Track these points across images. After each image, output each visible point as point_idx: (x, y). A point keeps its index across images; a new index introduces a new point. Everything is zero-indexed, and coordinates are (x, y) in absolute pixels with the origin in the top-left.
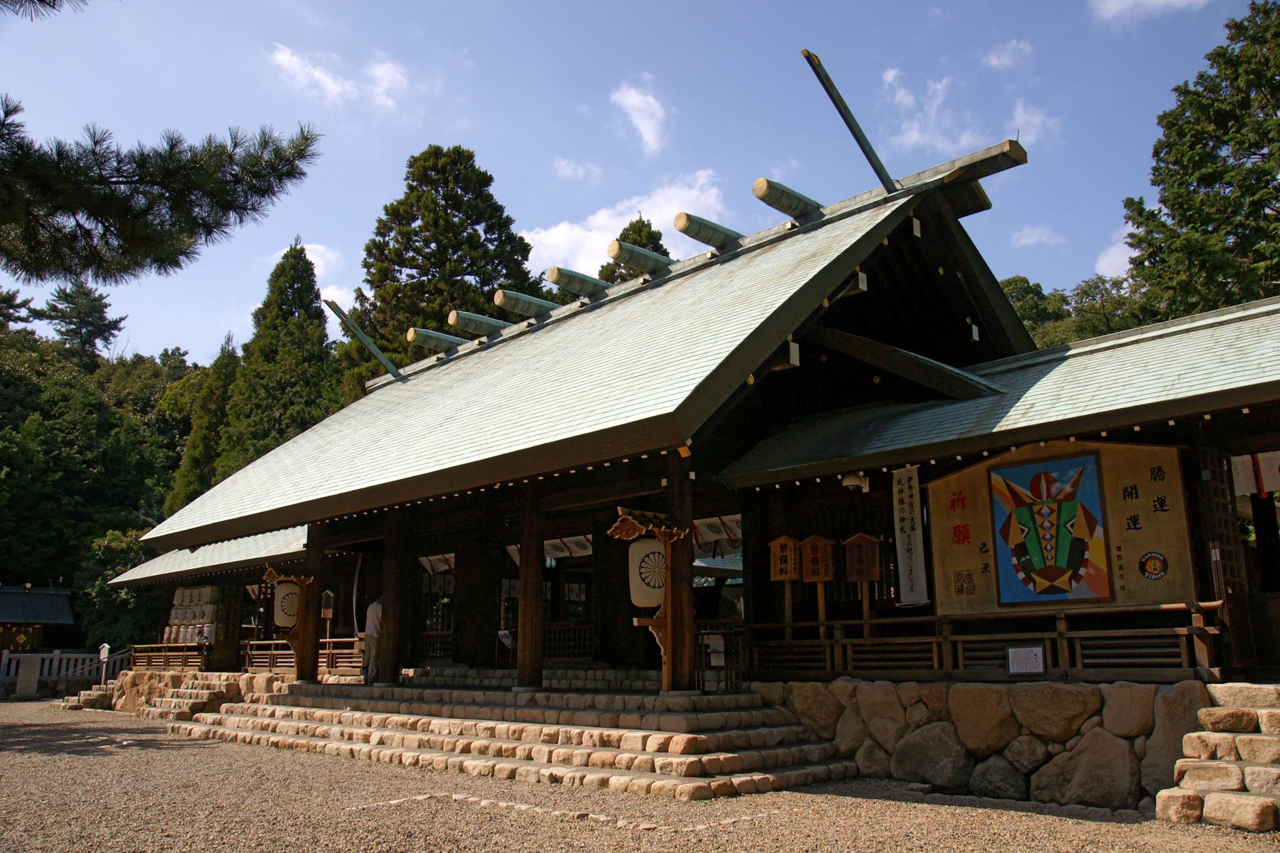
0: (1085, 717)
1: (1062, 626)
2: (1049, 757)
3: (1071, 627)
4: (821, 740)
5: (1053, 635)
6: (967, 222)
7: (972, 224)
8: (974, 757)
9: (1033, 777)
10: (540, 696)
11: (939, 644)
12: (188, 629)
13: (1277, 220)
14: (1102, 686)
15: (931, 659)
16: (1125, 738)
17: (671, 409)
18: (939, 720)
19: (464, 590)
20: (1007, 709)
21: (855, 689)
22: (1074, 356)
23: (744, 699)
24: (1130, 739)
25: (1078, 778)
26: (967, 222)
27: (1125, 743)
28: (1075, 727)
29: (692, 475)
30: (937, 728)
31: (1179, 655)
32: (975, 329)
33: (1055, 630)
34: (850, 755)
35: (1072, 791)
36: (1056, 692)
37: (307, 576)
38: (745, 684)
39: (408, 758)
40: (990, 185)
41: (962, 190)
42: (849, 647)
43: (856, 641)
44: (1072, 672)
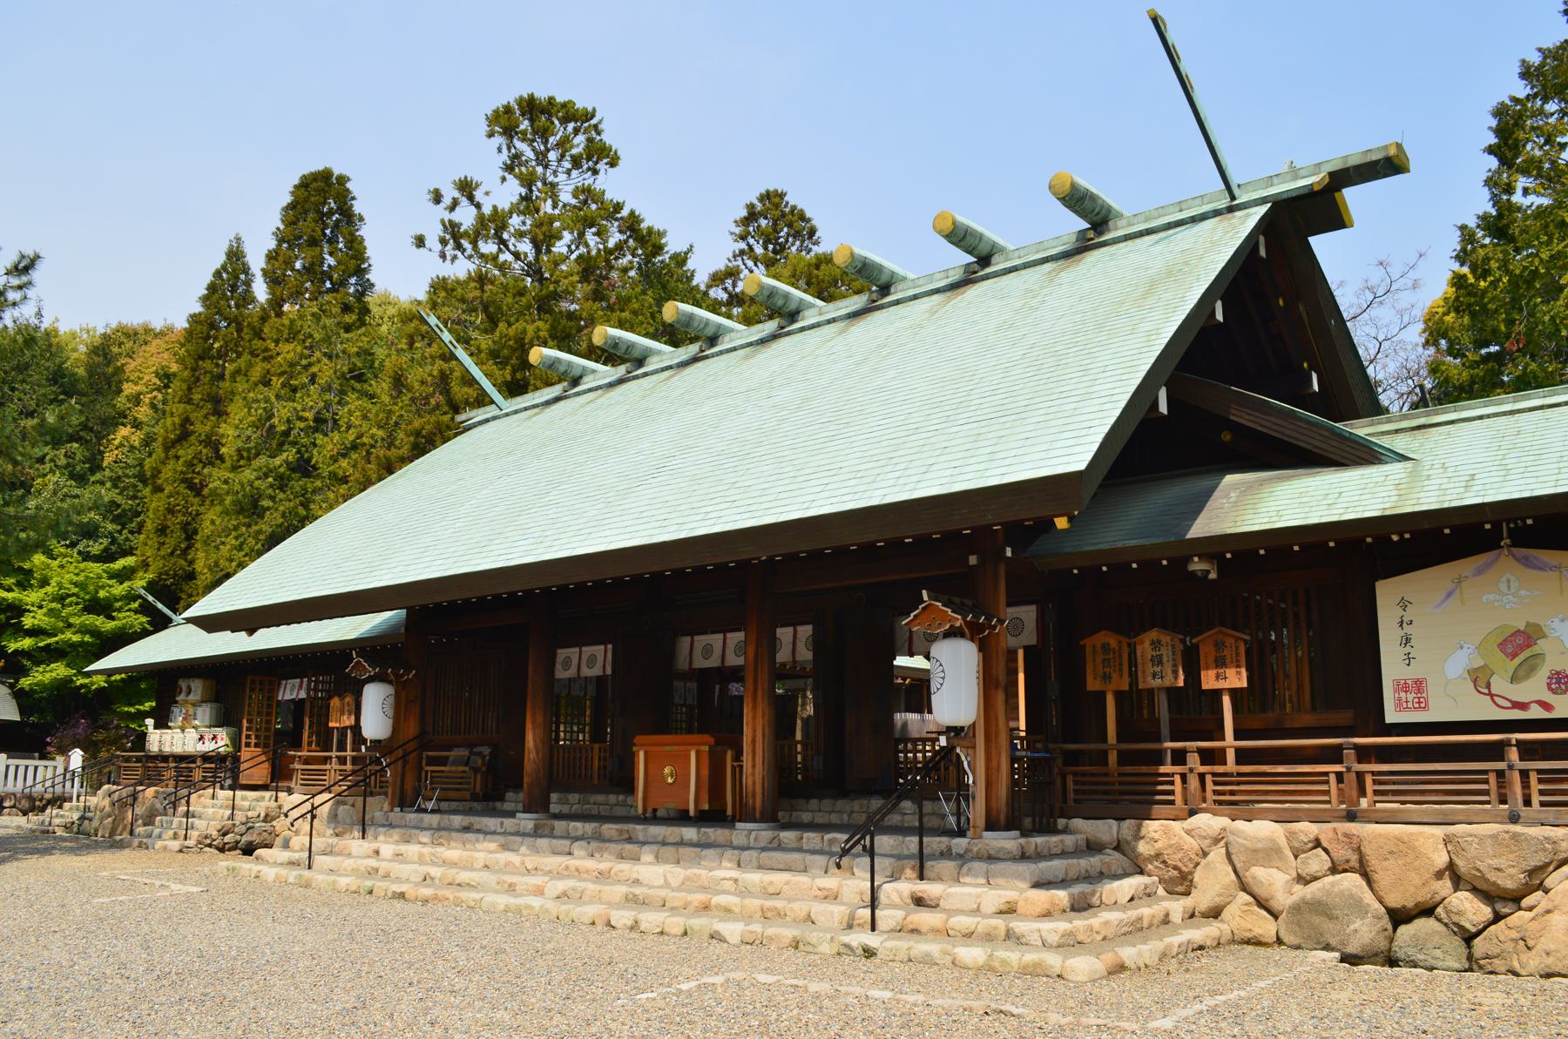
1: (1513, 754)
5: (1501, 765)
6: (1319, 243)
7: (1322, 245)
8: (1399, 917)
10: (788, 836)
11: (1184, 777)
17: (1082, 466)
19: (538, 698)
23: (1069, 840)
26: (1319, 243)
29: (1009, 553)
36: (1515, 836)
37: (408, 671)
38: (1061, 822)
39: (622, 918)
40: (1353, 197)
41: (1311, 210)
43: (1220, 769)
44: (1524, 812)
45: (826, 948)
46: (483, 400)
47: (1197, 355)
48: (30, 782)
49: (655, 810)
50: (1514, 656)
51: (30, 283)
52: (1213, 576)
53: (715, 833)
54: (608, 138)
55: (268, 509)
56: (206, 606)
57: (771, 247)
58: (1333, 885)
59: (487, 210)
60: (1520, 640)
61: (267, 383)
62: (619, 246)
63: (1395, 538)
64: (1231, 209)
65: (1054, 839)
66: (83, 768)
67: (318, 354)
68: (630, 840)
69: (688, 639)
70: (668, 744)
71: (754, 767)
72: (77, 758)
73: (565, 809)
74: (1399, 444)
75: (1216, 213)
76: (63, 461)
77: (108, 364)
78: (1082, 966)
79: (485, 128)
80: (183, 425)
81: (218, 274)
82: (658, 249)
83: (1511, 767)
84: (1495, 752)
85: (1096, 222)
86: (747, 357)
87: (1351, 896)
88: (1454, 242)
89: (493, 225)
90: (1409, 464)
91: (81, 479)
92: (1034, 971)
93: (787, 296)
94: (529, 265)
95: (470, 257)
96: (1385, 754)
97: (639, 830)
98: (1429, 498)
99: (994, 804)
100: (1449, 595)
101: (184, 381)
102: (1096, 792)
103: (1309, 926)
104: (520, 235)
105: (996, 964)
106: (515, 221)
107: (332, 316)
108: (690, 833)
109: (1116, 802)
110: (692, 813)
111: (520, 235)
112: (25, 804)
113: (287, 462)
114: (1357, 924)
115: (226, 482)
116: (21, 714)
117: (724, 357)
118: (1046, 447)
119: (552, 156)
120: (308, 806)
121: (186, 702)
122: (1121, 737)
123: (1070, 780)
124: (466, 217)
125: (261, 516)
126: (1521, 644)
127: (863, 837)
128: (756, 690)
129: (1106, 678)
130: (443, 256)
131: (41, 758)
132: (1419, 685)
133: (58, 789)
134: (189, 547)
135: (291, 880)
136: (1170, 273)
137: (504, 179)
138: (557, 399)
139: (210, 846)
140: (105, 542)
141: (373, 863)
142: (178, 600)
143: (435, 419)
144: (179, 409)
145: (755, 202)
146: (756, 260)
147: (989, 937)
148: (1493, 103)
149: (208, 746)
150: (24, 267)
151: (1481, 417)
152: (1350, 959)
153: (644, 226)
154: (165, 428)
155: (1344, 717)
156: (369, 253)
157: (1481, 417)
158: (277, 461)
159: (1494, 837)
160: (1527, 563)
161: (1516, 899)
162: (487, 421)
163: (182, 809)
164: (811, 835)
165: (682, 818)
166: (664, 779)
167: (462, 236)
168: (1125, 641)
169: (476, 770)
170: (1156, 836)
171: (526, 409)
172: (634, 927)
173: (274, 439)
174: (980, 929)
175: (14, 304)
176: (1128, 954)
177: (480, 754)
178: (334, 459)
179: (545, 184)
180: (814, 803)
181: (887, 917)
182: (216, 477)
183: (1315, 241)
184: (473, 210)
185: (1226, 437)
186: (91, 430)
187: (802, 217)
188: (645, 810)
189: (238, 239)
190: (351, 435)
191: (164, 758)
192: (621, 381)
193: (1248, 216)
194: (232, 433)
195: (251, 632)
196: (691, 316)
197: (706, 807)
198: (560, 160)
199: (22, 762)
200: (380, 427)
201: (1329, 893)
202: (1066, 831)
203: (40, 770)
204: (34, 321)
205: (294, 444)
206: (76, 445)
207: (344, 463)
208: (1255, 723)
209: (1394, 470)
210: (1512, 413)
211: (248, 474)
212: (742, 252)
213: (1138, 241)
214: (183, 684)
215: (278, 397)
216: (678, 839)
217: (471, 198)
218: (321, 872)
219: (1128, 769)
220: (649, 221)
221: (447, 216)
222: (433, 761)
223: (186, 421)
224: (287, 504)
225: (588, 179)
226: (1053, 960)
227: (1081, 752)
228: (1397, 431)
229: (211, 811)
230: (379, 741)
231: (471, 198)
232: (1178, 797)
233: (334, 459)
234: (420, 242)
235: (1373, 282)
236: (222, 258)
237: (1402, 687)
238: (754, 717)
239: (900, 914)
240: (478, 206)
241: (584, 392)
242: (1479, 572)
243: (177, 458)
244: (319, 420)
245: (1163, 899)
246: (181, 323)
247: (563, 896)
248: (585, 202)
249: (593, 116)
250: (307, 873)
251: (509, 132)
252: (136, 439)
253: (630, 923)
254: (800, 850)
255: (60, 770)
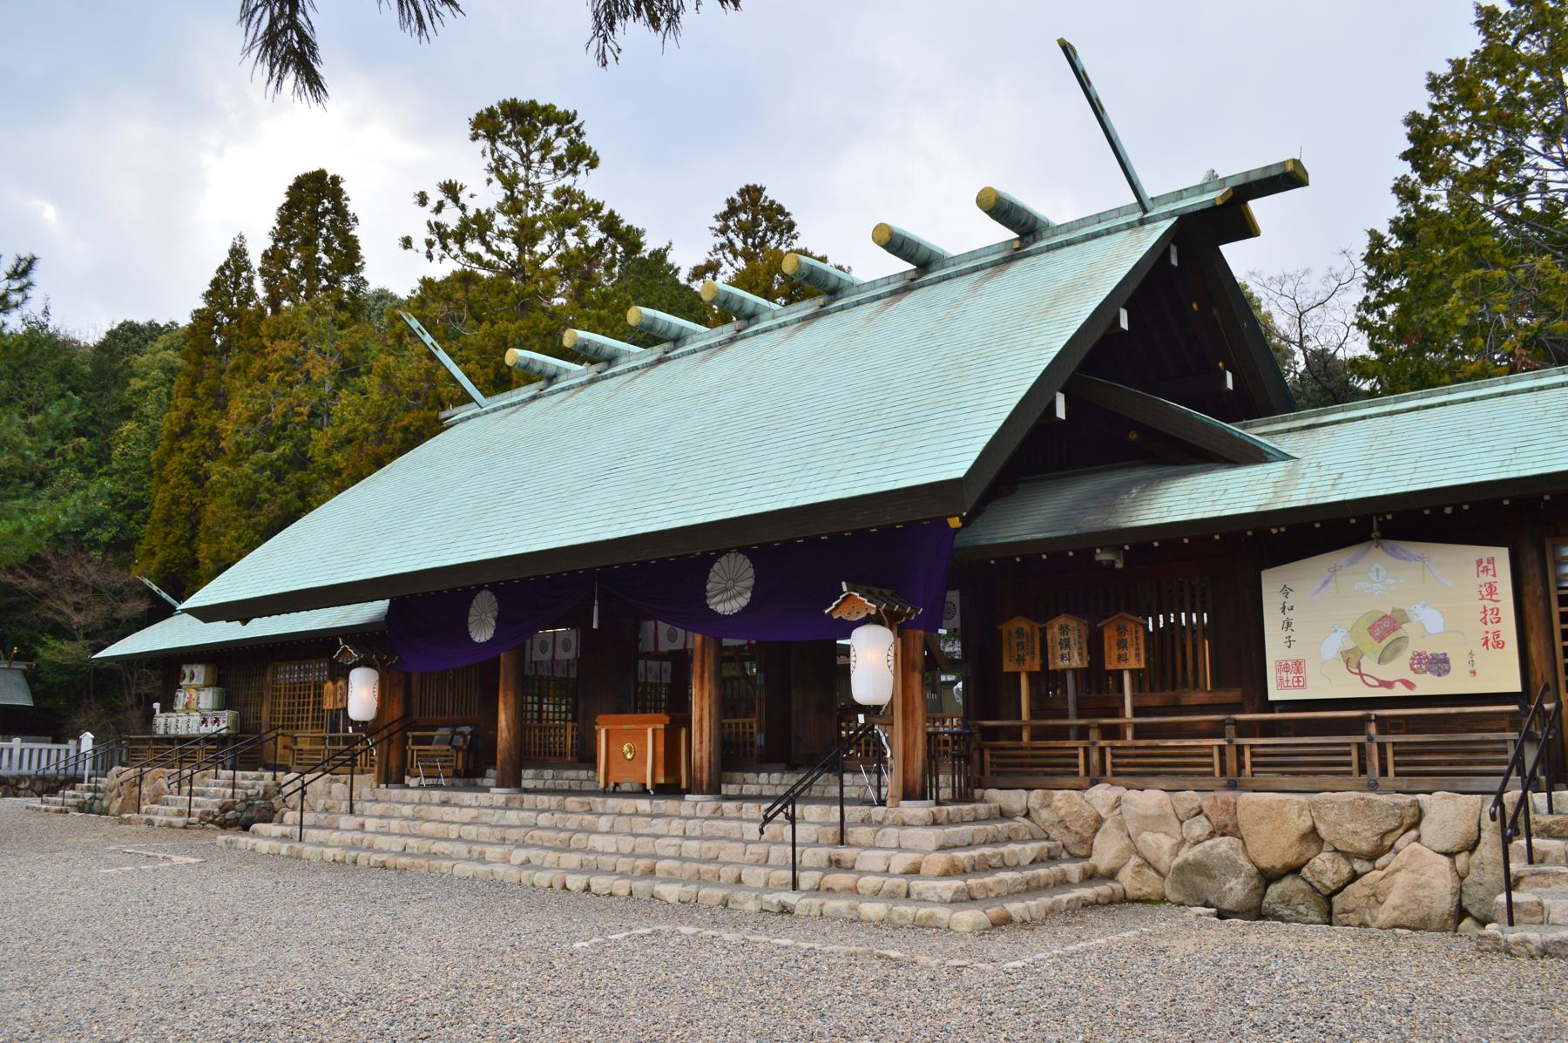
0: (1400, 831)
1: (1372, 729)
2: (1355, 876)
3: (1381, 732)
4: (1074, 857)
5: (1362, 739)
6: (1228, 250)
7: (1232, 252)
8: (1268, 877)
9: (1336, 898)
10: (729, 806)
11: (1086, 750)
12: (194, 711)
13: (5, 296)
14: (1420, 797)
15: (1212, 765)
16: (1445, 854)
17: (961, 474)
18: (1223, 835)
19: (537, 668)
20: (1309, 823)
21: (1119, 799)
22: (462, 420)
23: (981, 808)
24: (1450, 854)
25: (1393, 899)
26: (1228, 250)
27: (1445, 860)
28: (1387, 843)
30: (1223, 844)
31: (1349, 764)
32: (1229, 376)
33: (1362, 733)
34: (1111, 875)
35: (1384, 915)
36: (1369, 803)
38: (978, 792)
39: (575, 882)
41: (1228, 215)
42: (1108, 751)
43: (1118, 743)
44: (1382, 781)
45: (751, 906)
46: (468, 399)
47: (1094, 359)
48: (44, 765)
49: (616, 784)
50: (1381, 639)
51: (30, 284)
52: (1119, 565)
53: (666, 805)
54: (588, 140)
55: (265, 501)
56: (206, 596)
57: (750, 241)
58: (1212, 847)
59: (471, 213)
60: (1387, 625)
61: (263, 379)
62: (600, 244)
63: (1274, 531)
64: (1142, 222)
65: (966, 807)
66: (95, 751)
67: (311, 351)
68: (590, 811)
69: (652, 623)
70: (628, 723)
71: (701, 743)
72: (87, 739)
73: (540, 784)
74: (1286, 444)
75: (1130, 226)
76: (71, 455)
77: (114, 361)
78: (968, 917)
79: (469, 132)
80: (187, 419)
81: (221, 270)
82: (638, 246)
83: (1371, 739)
84: (1356, 727)
85: (1025, 230)
86: (703, 360)
87: (1228, 858)
88: (1362, 245)
89: (477, 226)
90: (1290, 463)
91: (87, 471)
92: (920, 925)
93: (742, 300)
94: (513, 264)
95: (455, 257)
96: (1269, 729)
97: (597, 802)
98: (1301, 494)
99: (910, 776)
100: (1326, 582)
101: (188, 375)
102: (1022, 765)
103: (1192, 885)
104: (502, 235)
105: (895, 917)
106: (501, 222)
107: (325, 313)
108: (643, 805)
109: (1029, 774)
110: (649, 786)
111: (502, 235)
112: (39, 786)
113: (282, 455)
114: (1233, 883)
115: (225, 475)
116: (35, 696)
117: (684, 360)
118: (936, 455)
119: (535, 156)
120: (298, 783)
121: (190, 686)
122: (1034, 714)
123: (987, 753)
124: (451, 218)
125: (260, 508)
126: (1387, 628)
127: (785, 806)
128: (703, 673)
129: (1021, 660)
130: (430, 257)
131: (54, 742)
132: (1299, 666)
133: (71, 771)
134: (193, 537)
135: (284, 852)
136: (1076, 286)
137: (490, 181)
138: (534, 398)
139: (212, 822)
140: (114, 530)
141: (358, 835)
142: (183, 588)
143: (414, 419)
144: (186, 403)
145: (736, 197)
146: (735, 254)
147: (892, 896)
148: (1405, 113)
149: (211, 729)
150: (22, 270)
151: (1364, 418)
152: (1222, 915)
153: (624, 225)
154: (169, 422)
155: (1232, 695)
156: (362, 252)
157: (1364, 418)
158: (274, 455)
159: (1351, 803)
160: (1393, 553)
161: (1372, 857)
162: (469, 418)
163: (186, 788)
164: (749, 805)
165: (643, 792)
166: (624, 755)
167: (449, 236)
168: (1037, 625)
169: (458, 749)
170: (1060, 804)
171: (504, 407)
172: (587, 889)
173: (271, 433)
174: (886, 887)
175: (17, 306)
176: (1015, 908)
177: (461, 733)
178: (329, 453)
179: (527, 185)
180: (738, 776)
181: (807, 879)
182: (217, 471)
183: (1223, 248)
184: (458, 213)
185: (1133, 436)
186: (99, 424)
187: (780, 210)
188: (606, 784)
189: (241, 237)
190: (343, 431)
191: (170, 740)
192: (592, 381)
193: (1155, 229)
194: (230, 429)
195: (245, 622)
196: (655, 319)
197: (662, 780)
198: (543, 159)
199: (37, 746)
200: (371, 421)
201: (1208, 855)
202: (982, 800)
203: (54, 753)
204: (42, 319)
205: (291, 437)
206: (83, 440)
207: (338, 457)
208: (1154, 699)
209: (1276, 469)
210: (1391, 413)
211: (247, 468)
212: (723, 246)
213: (1058, 252)
214: (187, 670)
215: (274, 392)
216: (633, 810)
217: (456, 200)
218: (311, 844)
219: (1038, 743)
220: (628, 219)
221: (434, 218)
222: (417, 741)
223: (191, 414)
224: (284, 497)
225: (568, 181)
226: (943, 913)
227: (1002, 727)
228: (1289, 431)
229: (212, 789)
230: (365, 723)
231: (456, 200)
232: (1081, 770)
233: (329, 453)
234: (407, 243)
235: (1338, 268)
236: (226, 256)
237: (1285, 667)
238: (702, 698)
239: (817, 875)
240: (463, 208)
241: (558, 391)
242: (1352, 562)
243: (182, 450)
244: (313, 414)
245: (1064, 861)
246: (185, 321)
247: (526, 863)
248: (565, 203)
249: (574, 118)
250: (298, 846)
251: (492, 136)
252: (142, 434)
253: (583, 886)
254: (740, 819)
255: (72, 753)
